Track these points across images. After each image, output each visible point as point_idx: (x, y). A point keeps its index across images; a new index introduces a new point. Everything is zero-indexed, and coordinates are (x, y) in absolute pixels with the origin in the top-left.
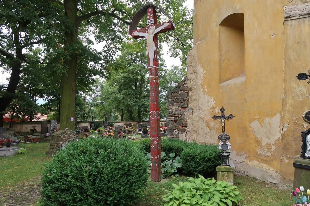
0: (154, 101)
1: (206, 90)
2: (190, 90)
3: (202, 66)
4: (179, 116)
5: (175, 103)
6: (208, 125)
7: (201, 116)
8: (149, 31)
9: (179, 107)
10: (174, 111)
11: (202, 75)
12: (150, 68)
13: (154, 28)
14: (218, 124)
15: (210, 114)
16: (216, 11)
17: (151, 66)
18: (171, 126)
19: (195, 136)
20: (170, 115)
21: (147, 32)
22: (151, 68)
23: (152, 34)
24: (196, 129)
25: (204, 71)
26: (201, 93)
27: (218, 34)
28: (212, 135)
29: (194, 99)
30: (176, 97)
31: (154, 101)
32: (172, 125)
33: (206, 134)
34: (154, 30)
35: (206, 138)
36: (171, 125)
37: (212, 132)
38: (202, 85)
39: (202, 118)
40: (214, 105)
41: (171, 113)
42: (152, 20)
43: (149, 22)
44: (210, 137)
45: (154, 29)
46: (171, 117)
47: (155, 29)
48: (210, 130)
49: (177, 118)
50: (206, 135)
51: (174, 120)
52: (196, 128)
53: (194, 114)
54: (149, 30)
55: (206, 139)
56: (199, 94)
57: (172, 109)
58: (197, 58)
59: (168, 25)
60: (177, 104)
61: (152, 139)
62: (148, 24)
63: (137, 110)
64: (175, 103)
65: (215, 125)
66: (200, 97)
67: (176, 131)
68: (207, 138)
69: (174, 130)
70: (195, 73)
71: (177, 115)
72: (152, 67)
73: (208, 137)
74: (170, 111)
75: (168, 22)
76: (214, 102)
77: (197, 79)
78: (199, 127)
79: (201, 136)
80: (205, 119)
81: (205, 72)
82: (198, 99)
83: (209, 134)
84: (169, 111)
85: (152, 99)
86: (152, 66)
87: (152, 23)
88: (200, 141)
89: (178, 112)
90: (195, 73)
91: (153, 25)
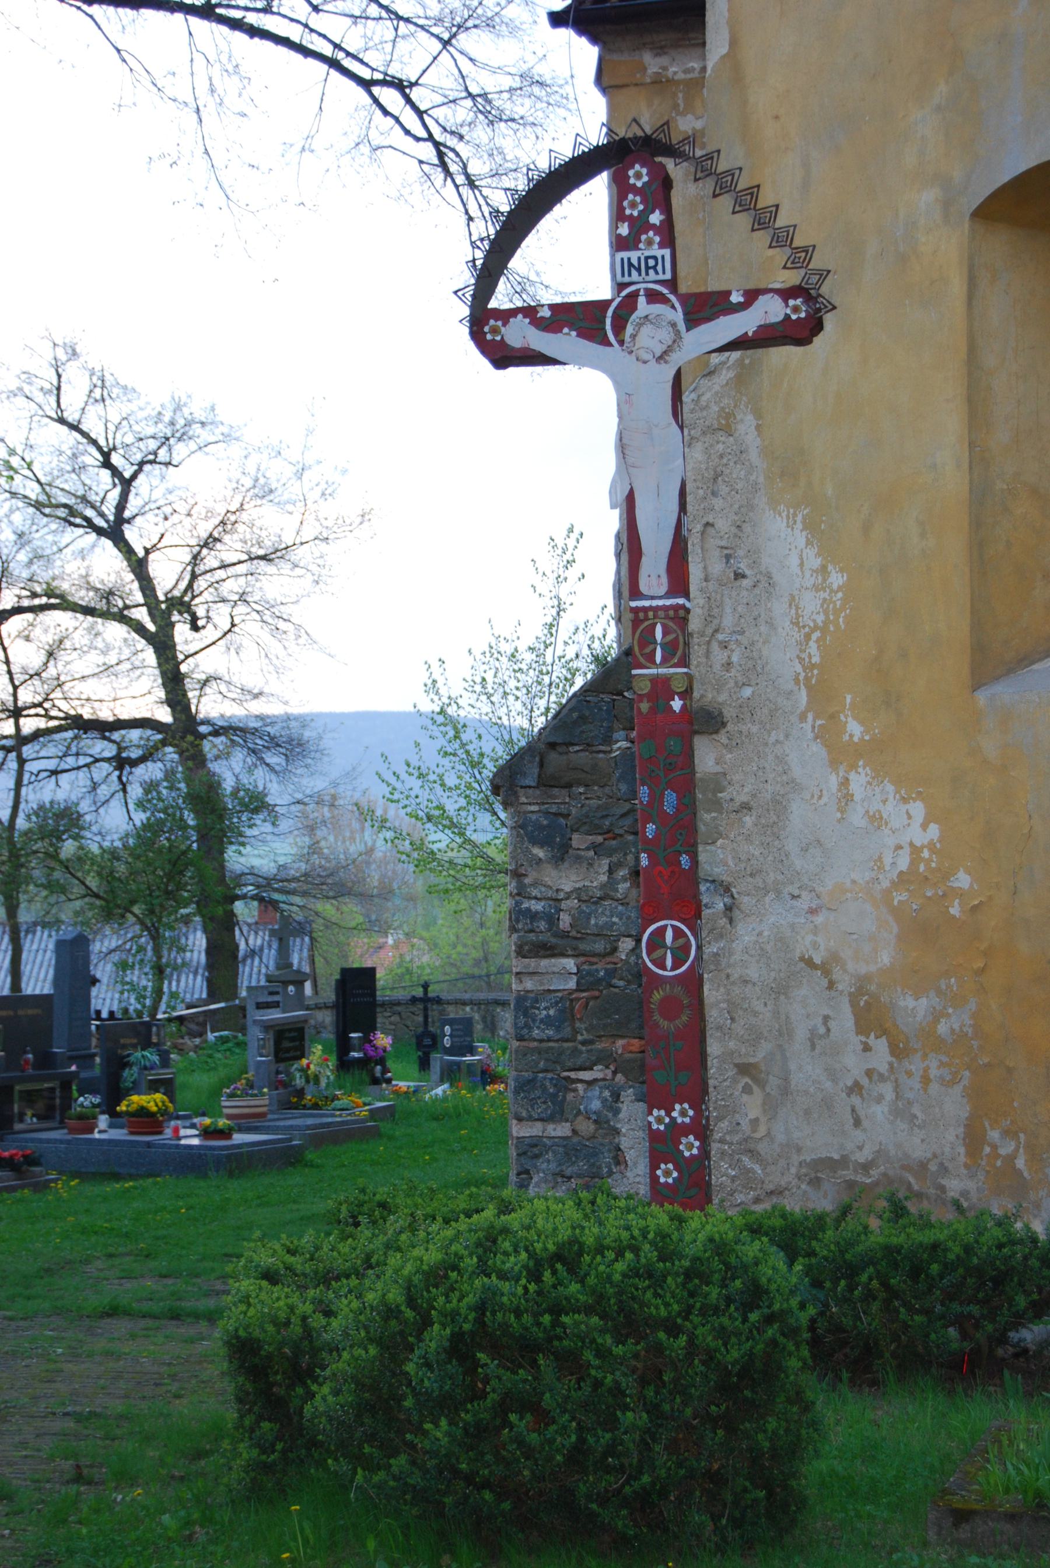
0: (678, 847)
1: (854, 729)
2: (709, 721)
3: (809, 526)
4: (615, 950)
5: (578, 840)
6: (871, 1017)
7: (804, 944)
8: (634, 337)
9: (611, 871)
10: (568, 911)
11: (811, 606)
12: (645, 610)
13: (679, 316)
14: (972, 1005)
15: (895, 930)
16: (942, 89)
17: (653, 598)
18: (549, 1040)
19: (752, 1115)
20: (533, 944)
21: (621, 343)
22: (651, 608)
23: (661, 358)
24: (760, 1055)
25: (830, 568)
26: (804, 754)
27: (957, 287)
28: (910, 1095)
29: (744, 798)
30: (579, 783)
31: (678, 847)
32: (558, 1029)
33: (856, 1088)
34: (678, 333)
35: (857, 1123)
36: (550, 1032)
37: (909, 1074)
38: (810, 688)
39: (818, 960)
40: (926, 854)
41: (542, 925)
42: (655, 258)
43: (630, 265)
44: (897, 1113)
45: (674, 325)
46: (544, 962)
47: (682, 326)
48: (899, 1051)
49: (601, 969)
50: (856, 1100)
51: (572, 984)
52: (765, 1048)
53: (741, 928)
54: (630, 329)
55: (858, 1132)
56: (780, 760)
57: (550, 894)
58: (754, 456)
59: (787, 317)
60: (595, 847)
61: (659, 1120)
62: (627, 279)
63: (29, 879)
65: (937, 1016)
66: (794, 786)
67: (596, 1080)
68: (865, 1123)
69: (572, 1075)
70: (739, 576)
71: (599, 946)
72: (655, 603)
73: (880, 1111)
74: (537, 906)
75: (786, 294)
76: (934, 831)
77: (763, 628)
78: (785, 1032)
79: (807, 1112)
80: (851, 966)
81: (837, 579)
82: (779, 805)
83: (887, 1090)
84: (528, 910)
85: (657, 835)
86: (660, 598)
87: (661, 277)
88: (799, 1150)
89: (604, 919)
90: (739, 576)
91: (665, 291)
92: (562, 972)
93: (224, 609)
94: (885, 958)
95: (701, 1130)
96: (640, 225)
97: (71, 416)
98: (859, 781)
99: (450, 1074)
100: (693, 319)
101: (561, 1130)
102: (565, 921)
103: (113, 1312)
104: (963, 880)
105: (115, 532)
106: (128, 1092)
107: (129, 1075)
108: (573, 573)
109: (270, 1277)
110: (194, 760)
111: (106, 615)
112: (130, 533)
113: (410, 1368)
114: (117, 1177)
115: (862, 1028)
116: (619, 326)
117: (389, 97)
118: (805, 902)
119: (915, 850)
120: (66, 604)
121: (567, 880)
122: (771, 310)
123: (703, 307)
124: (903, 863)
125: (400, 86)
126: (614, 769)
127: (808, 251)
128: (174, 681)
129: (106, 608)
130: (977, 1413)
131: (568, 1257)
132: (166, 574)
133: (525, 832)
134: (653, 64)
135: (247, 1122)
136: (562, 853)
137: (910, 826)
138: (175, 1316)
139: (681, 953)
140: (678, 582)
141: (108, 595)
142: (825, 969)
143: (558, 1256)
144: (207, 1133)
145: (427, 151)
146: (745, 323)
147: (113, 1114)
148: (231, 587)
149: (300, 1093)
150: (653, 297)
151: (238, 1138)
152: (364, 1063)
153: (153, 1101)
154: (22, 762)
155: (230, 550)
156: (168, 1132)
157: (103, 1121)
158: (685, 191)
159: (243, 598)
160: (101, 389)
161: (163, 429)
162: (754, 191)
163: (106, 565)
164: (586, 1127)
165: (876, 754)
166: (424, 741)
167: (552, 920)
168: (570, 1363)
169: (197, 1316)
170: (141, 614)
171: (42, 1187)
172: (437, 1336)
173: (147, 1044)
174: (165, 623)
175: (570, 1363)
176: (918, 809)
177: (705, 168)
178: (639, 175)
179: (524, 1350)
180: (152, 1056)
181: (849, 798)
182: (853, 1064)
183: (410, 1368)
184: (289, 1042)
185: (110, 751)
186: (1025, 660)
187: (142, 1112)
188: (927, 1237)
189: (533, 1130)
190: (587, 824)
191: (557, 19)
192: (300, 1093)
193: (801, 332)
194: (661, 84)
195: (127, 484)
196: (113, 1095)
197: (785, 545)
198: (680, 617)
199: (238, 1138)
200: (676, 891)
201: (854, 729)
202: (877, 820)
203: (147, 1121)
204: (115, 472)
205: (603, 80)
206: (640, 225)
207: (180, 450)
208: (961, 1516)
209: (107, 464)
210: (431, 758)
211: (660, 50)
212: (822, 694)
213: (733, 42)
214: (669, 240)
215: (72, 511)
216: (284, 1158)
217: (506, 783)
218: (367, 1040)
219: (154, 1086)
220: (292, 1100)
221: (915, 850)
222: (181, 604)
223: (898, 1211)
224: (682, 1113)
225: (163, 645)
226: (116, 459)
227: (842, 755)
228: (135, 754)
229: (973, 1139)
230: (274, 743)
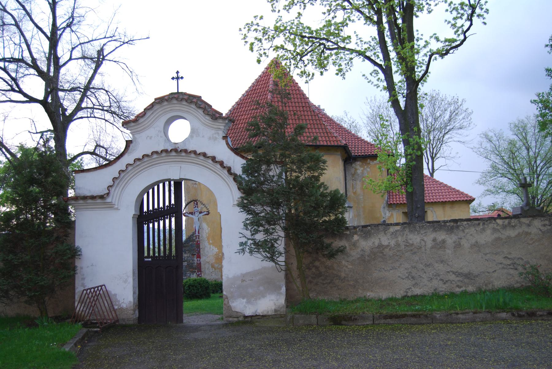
6: (213, 266)
11: (207, 231)
26: (206, 244)
82: (204, 248)
98: (211, 246)
122: (206, 213)
123: (201, 213)
131: (195, 280)
158: (199, 203)
165: (212, 244)
168: (196, 287)
175: (196, 287)
179: (193, 286)
182: (211, 271)
190: (187, 250)
193: (208, 214)
197: (205, 226)
200: (446, 295)
212: (208, 239)
227: (210, 244)
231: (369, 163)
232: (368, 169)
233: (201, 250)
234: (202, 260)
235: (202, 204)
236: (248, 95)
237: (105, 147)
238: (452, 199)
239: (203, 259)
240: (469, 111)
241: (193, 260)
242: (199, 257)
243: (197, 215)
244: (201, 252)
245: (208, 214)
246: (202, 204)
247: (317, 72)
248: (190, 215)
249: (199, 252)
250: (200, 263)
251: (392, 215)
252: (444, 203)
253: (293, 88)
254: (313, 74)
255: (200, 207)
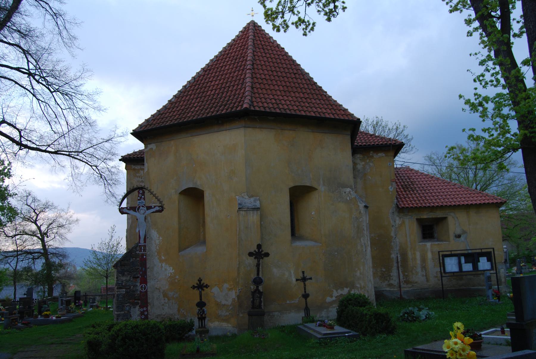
1: (163, 258)
5: (126, 273)
6: (165, 295)
11: (157, 242)
13: (146, 209)
27: (177, 202)
33: (163, 305)
48: (169, 300)
64: (126, 273)
75: (159, 207)
76: (173, 271)
81: (161, 238)
83: (167, 305)
92: (123, 291)
93: (53, 235)
94: (167, 287)
95: (147, 310)
96: (141, 198)
97: (29, 204)
99: (92, 307)
100: (147, 210)
101: (123, 313)
102: (124, 284)
103: (52, 344)
104: (177, 277)
105: (35, 222)
106: (44, 311)
107: (43, 309)
108: (114, 232)
109: (90, 334)
110: (47, 259)
111: (34, 236)
112: (38, 223)
113: (116, 342)
114: (43, 325)
115: (164, 296)
116: (138, 210)
117: (94, 167)
118: (156, 281)
119: (171, 273)
120: (26, 234)
121: (124, 278)
122: (157, 208)
123: (149, 208)
124: (170, 275)
125: (96, 167)
126: (133, 263)
127: (162, 202)
128: (44, 245)
129: (33, 234)
130: (182, 344)
131: (137, 326)
132: (43, 228)
133: (118, 272)
134: (133, 167)
135: (63, 315)
136: (123, 275)
137: (170, 270)
138: (62, 343)
139: (145, 288)
140: (145, 242)
141: (34, 232)
142: (159, 289)
143: (135, 327)
144: (57, 317)
145: (100, 175)
146: (154, 210)
147: (41, 315)
148: (55, 231)
149: (70, 310)
150: (142, 206)
151: (62, 318)
152: (79, 305)
153: (48, 313)
154: (18, 259)
155: (54, 225)
156: (50, 318)
157: (39, 317)
158: (146, 192)
159: (57, 233)
160: (34, 200)
161: (44, 207)
162: (162, 202)
163: (34, 227)
164: (126, 312)
166: (91, 256)
167: (122, 284)
169: (65, 343)
170: (39, 235)
171: (31, 327)
172: (120, 338)
173: (45, 304)
174: (43, 236)
176: (171, 268)
177: (149, 191)
178: (141, 192)
180: (46, 306)
181: (162, 267)
183: (116, 342)
184: (68, 303)
185: (31, 257)
186: (185, 249)
187: (46, 314)
188: (175, 323)
189: (119, 313)
191: (120, 160)
192: (70, 310)
194: (134, 169)
195: (38, 215)
196: (40, 313)
197: (154, 234)
198: (145, 246)
199: (62, 318)
201: (163, 258)
202: (166, 270)
203: (47, 316)
204: (36, 213)
205: (126, 168)
206: (141, 198)
207: (47, 210)
208: (184, 355)
209: (34, 212)
210: (92, 259)
211: (134, 165)
213: (148, 169)
214: (144, 200)
215: (29, 219)
216: (69, 320)
217: (115, 266)
218: (79, 302)
219: (47, 311)
220: (69, 312)
221: (171, 273)
222: (46, 234)
223: (170, 320)
224: (145, 309)
225: (43, 240)
226: (36, 211)
227: (161, 261)
228: (36, 257)
229: (179, 310)
230: (61, 255)
231: (372, 157)
232: (371, 164)
233: (148, 270)
234: (148, 285)
235: (152, 193)
236: (218, 60)
237: (18, 126)
238: (479, 202)
239: (151, 283)
240: (409, 137)
241: (135, 286)
242: (144, 281)
243: (142, 212)
244: (148, 274)
245: (161, 210)
246: (152, 193)
247: (320, 19)
248: (131, 212)
249: (145, 273)
250: (146, 292)
251: (403, 222)
252: (467, 207)
253: (279, 53)
254: (314, 24)
255: (149, 200)
